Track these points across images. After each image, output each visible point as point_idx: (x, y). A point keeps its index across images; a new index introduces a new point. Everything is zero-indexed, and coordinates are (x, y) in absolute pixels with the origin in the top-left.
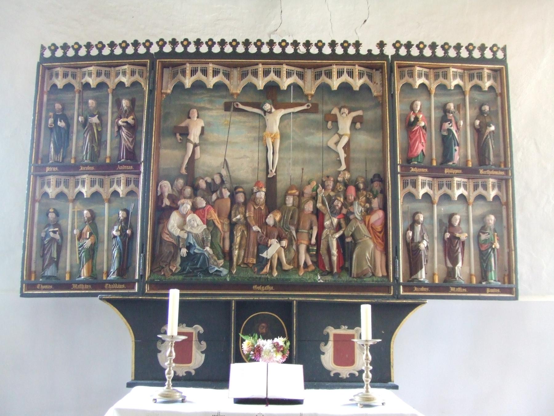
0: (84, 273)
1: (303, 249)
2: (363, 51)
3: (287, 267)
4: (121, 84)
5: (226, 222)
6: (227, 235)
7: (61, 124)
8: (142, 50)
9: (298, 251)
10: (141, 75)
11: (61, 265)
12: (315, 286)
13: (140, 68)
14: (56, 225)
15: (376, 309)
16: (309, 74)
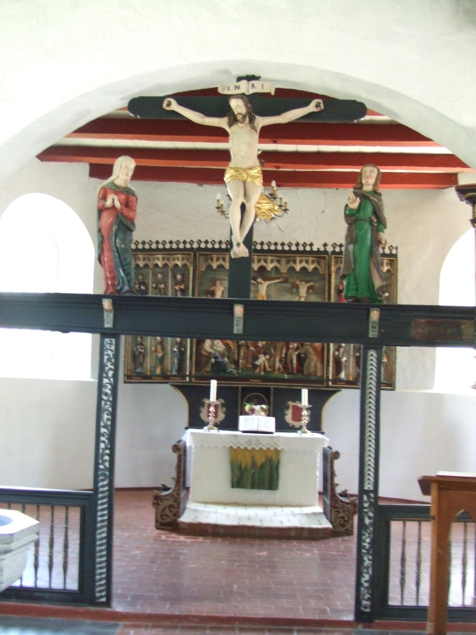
0: (158, 371)
1: (277, 360)
2: (315, 249)
3: (268, 369)
4: (176, 265)
5: (236, 344)
6: (236, 352)
7: (143, 288)
8: (188, 246)
9: (274, 362)
10: (188, 260)
11: (145, 366)
12: (284, 380)
13: (187, 256)
14: (142, 344)
15: (310, 393)
16: (283, 261)
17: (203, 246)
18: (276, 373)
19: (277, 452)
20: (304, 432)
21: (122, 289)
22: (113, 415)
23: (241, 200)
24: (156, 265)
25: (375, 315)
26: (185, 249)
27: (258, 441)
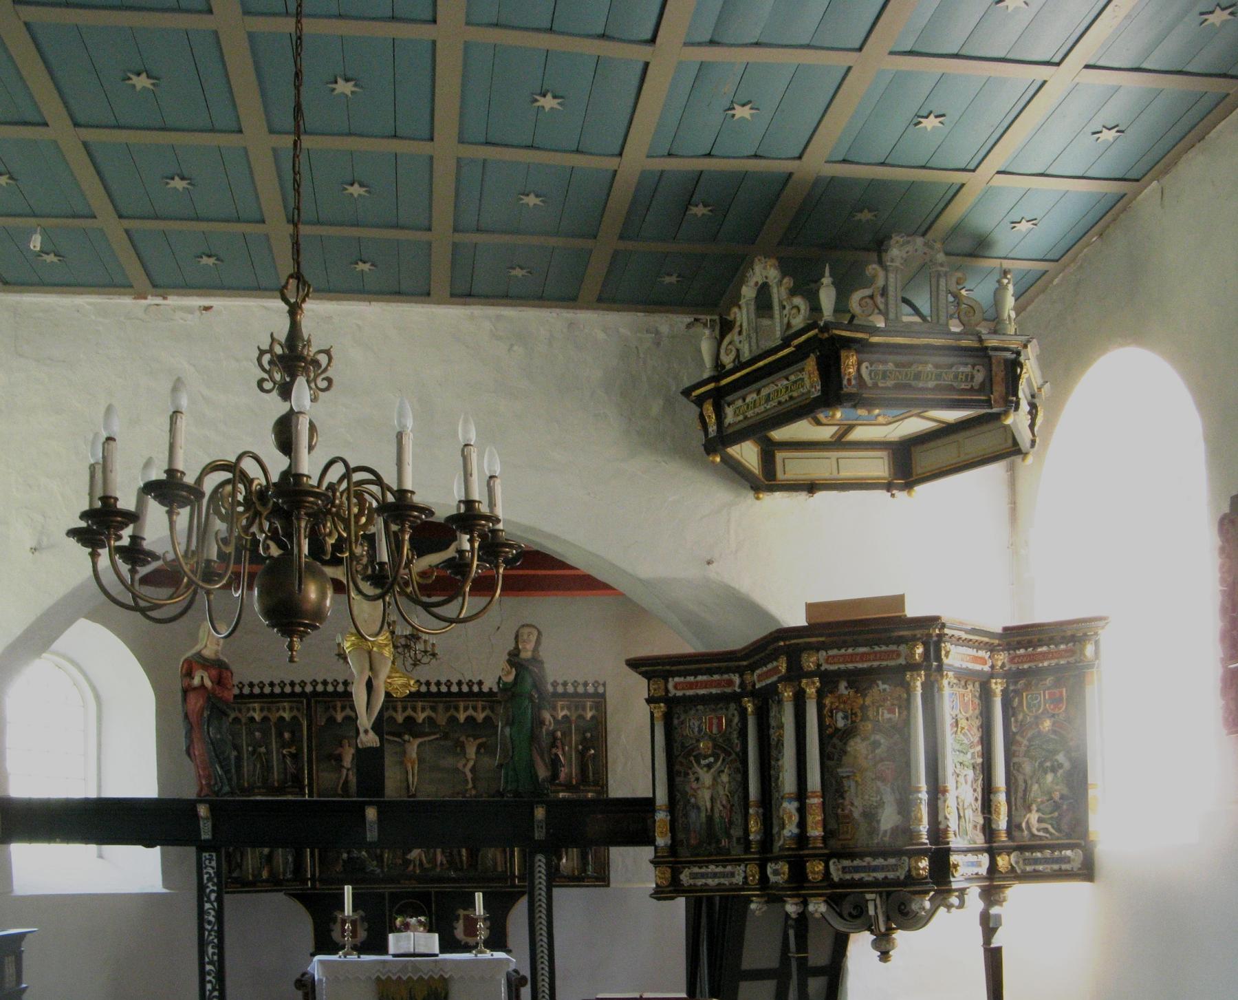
0: (265, 875)
2: (485, 689)
3: (427, 866)
4: (282, 718)
8: (298, 689)
10: (298, 710)
11: (244, 867)
16: (441, 707)
17: (320, 688)
18: (438, 870)
19: (444, 980)
20: (481, 952)
21: (220, 789)
22: (220, 947)
23: (367, 674)
24: (252, 719)
25: (540, 813)
26: (293, 694)
27: (415, 967)
